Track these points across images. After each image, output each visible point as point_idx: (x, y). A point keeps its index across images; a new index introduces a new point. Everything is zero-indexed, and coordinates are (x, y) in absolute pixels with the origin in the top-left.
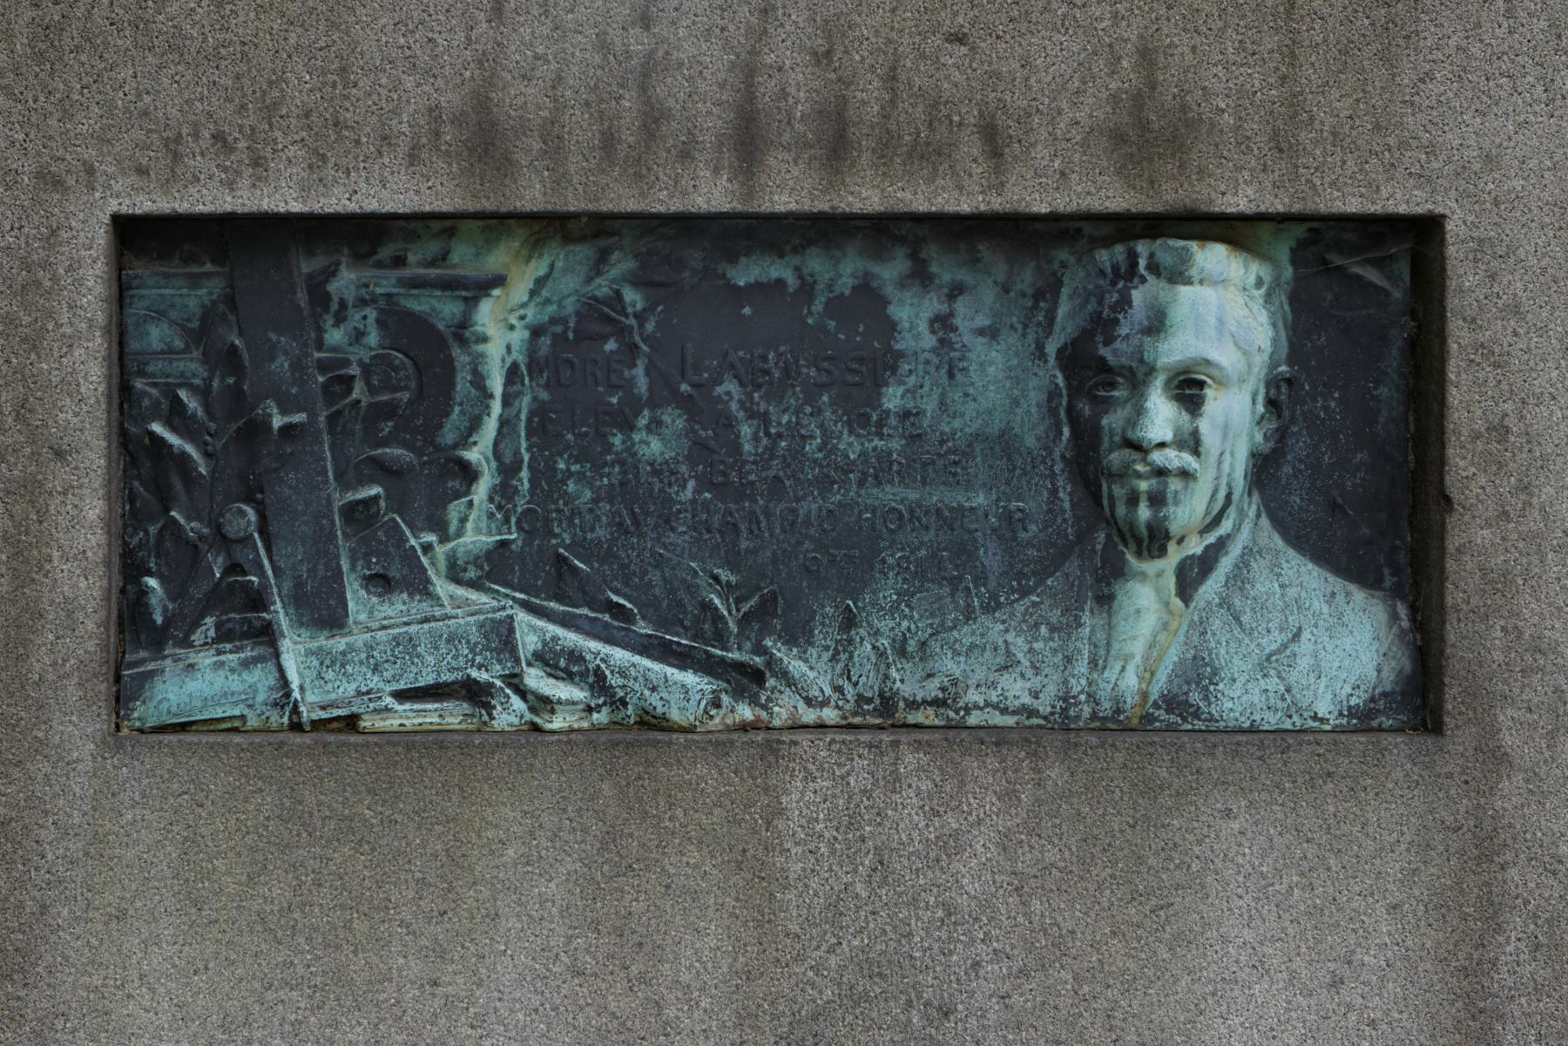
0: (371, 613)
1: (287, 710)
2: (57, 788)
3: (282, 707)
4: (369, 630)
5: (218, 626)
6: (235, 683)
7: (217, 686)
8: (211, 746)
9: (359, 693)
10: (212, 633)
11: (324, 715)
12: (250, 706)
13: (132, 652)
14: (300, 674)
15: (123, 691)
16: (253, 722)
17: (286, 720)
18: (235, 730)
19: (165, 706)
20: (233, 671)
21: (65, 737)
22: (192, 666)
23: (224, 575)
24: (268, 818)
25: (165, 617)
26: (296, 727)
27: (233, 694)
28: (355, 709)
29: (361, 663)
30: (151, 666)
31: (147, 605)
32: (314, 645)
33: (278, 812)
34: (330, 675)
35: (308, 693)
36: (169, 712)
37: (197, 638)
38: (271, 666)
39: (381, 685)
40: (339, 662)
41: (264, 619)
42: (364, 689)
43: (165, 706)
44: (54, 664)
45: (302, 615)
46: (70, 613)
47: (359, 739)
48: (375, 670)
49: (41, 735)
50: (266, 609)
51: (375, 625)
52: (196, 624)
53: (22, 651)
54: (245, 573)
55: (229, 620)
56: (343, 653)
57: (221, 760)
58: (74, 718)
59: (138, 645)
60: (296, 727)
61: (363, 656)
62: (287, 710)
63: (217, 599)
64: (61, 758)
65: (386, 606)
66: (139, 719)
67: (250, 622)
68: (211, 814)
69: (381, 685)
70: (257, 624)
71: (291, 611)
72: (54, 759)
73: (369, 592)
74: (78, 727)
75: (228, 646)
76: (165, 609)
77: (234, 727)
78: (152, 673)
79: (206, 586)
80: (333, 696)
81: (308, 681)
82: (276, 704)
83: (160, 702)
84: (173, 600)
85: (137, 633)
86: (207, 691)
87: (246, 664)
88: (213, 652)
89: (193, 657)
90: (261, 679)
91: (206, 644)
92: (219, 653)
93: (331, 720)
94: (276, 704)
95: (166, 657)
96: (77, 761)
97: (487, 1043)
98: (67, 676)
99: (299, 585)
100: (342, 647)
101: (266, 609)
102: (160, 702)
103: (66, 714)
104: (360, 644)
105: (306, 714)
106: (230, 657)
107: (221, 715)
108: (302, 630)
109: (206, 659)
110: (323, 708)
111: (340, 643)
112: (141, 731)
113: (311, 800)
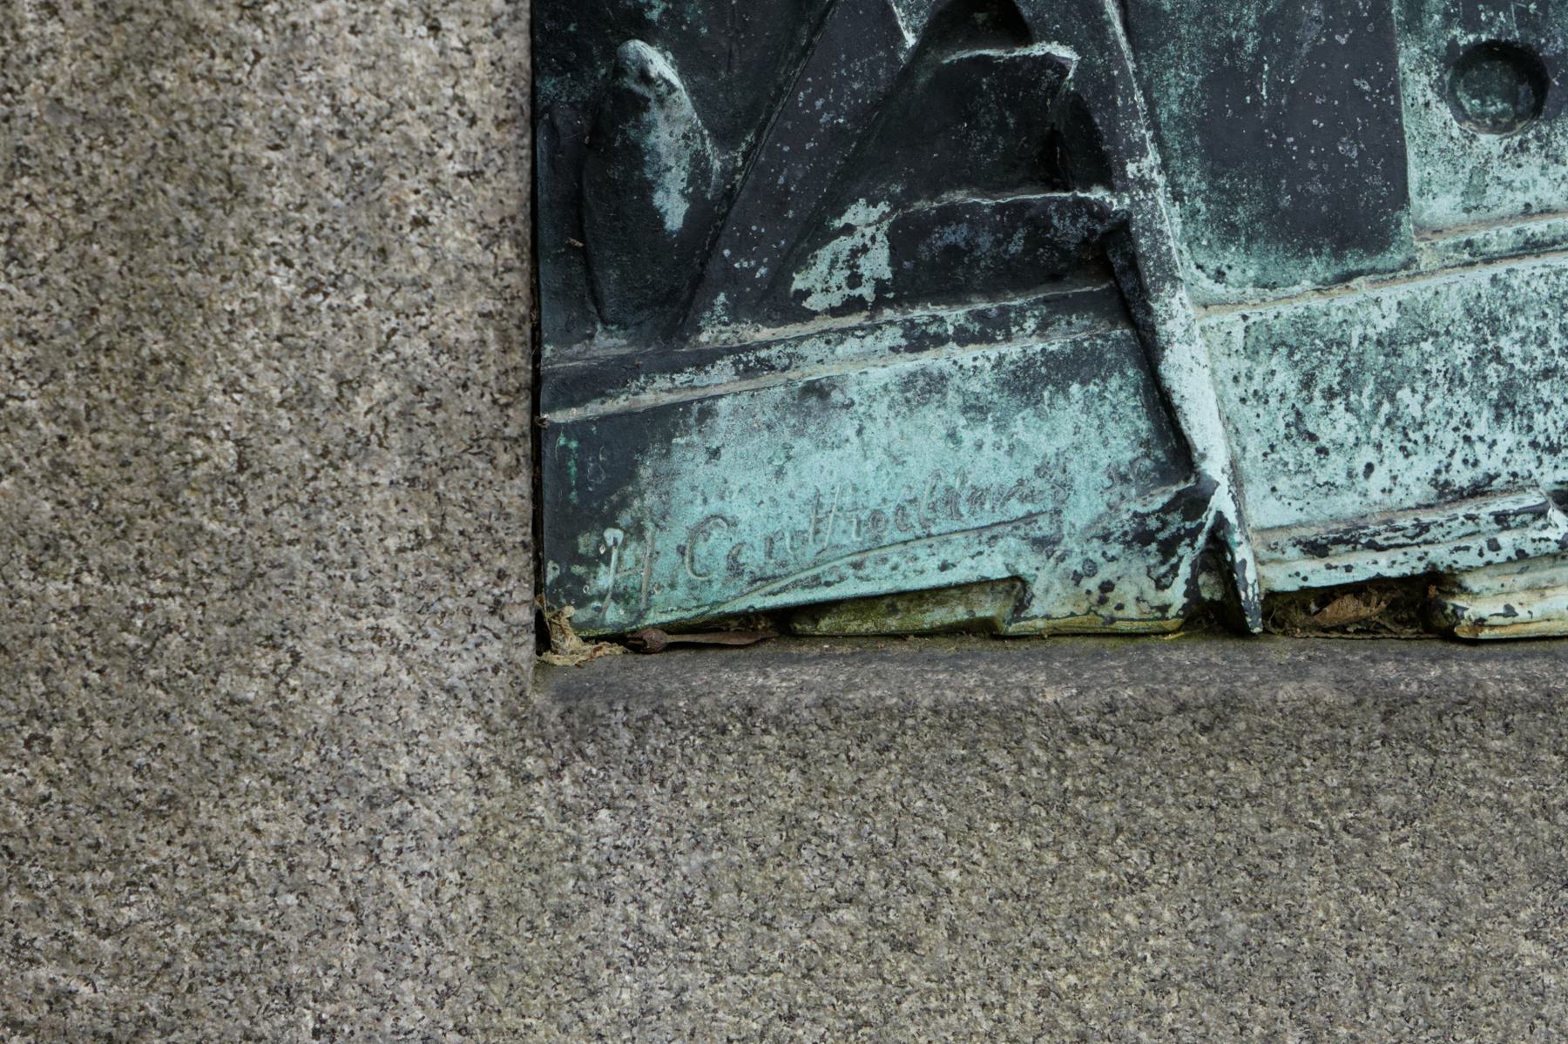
0: (1475, 190)
1: (1186, 556)
2: (330, 898)
3: (1168, 549)
4: (1477, 255)
5: (903, 238)
6: (989, 459)
7: (918, 470)
8: (953, 720)
9: (1446, 493)
10: (877, 264)
11: (1319, 574)
12: (1043, 544)
13: (565, 337)
14: (1233, 430)
15: (575, 490)
16: (1052, 601)
17: (1176, 595)
18: (986, 630)
19: (718, 545)
20: (975, 409)
21: (358, 697)
22: (818, 391)
23: (933, 36)
24: (1159, 985)
25: (695, 199)
26: (1218, 616)
27: (977, 497)
28: (1440, 555)
29: (1455, 379)
30: (655, 393)
31: (635, 155)
32: (1282, 311)
33: (1197, 958)
34: (1337, 425)
35: (1255, 491)
36: (735, 569)
37: (819, 280)
38: (1121, 389)
39: (1524, 462)
40: (1363, 375)
41: (1099, 213)
42: (1462, 477)
43: (718, 545)
44: (301, 399)
45: (1233, 199)
46: (363, 182)
47: (1490, 675)
48: (1504, 407)
49: (253, 690)
50: (1105, 172)
51: (1503, 237)
52: (817, 232)
53: (154, 342)
54: (1024, 35)
55: (949, 215)
56: (1390, 344)
57: (989, 773)
58: (393, 622)
59: (589, 305)
60: (1218, 616)
61: (1463, 353)
62: (1186, 556)
63: (902, 136)
64: (342, 784)
65: (1533, 162)
66: (620, 596)
67: (1037, 224)
68: (945, 975)
69: (1524, 462)
70: (1069, 230)
71: (1193, 181)
72: (318, 781)
73: (1460, 114)
74: (405, 661)
75: (953, 316)
76: (699, 171)
77: (985, 624)
78: (662, 424)
79: (858, 80)
80: (1347, 504)
81: (1255, 445)
82: (1142, 537)
83: (699, 531)
84: (725, 137)
85: (613, 267)
86: (881, 490)
87: (1025, 384)
88: (893, 336)
89: (817, 362)
90: (1088, 437)
91: (852, 305)
92: (918, 340)
93: (1327, 595)
94: (1142, 537)
95: (705, 359)
96: (411, 789)
97: (923, 1040)
98: (359, 447)
99: (1226, 76)
100: (1384, 321)
101: (1105, 172)
102: (699, 531)
103: (357, 606)
104: (1451, 307)
105: (1263, 572)
106: (967, 355)
107: (934, 579)
108: (1231, 256)
109: (869, 365)
110: (1316, 549)
111: (1371, 306)
112: (631, 641)
113: (1322, 911)
